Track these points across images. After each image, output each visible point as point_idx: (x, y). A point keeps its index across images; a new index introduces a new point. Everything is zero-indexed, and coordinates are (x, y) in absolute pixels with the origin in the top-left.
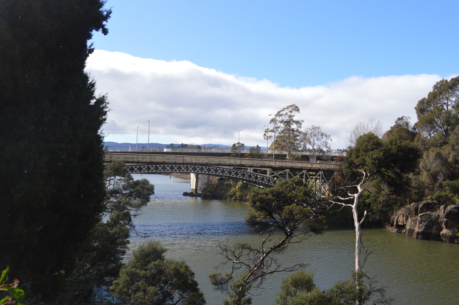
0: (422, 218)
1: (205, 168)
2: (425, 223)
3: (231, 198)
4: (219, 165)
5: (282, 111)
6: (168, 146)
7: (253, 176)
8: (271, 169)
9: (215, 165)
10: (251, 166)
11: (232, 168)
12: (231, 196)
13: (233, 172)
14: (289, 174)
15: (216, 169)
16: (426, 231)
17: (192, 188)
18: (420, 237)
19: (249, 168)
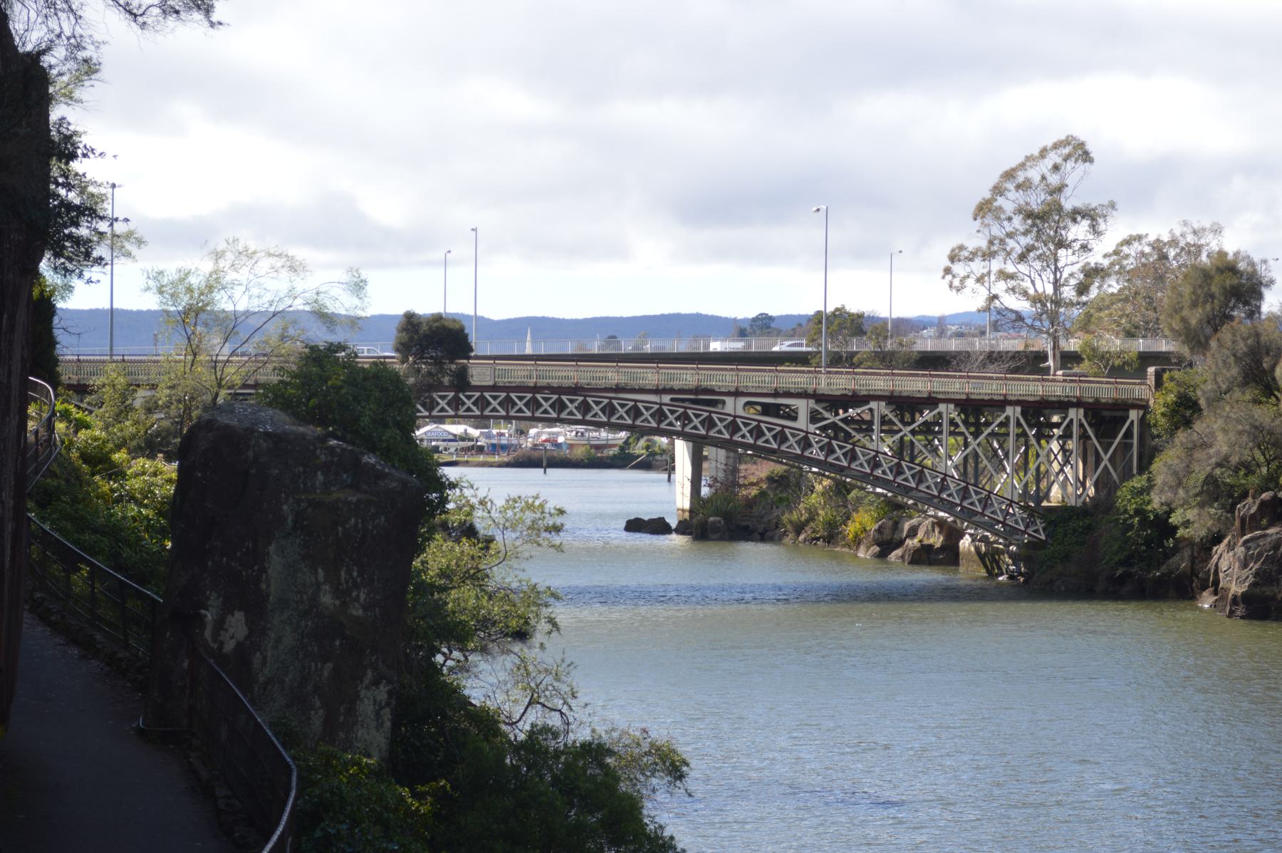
0: (1248, 549)
1: (572, 401)
2: (1257, 566)
3: (798, 533)
4: (618, 389)
5: (1022, 166)
6: (743, 329)
7: (746, 425)
8: (812, 402)
9: (606, 390)
10: (737, 393)
11: (666, 399)
12: (799, 528)
13: (672, 412)
14: (884, 421)
15: (611, 406)
16: (1258, 590)
17: (679, 505)
18: (1238, 613)
19: (729, 401)
